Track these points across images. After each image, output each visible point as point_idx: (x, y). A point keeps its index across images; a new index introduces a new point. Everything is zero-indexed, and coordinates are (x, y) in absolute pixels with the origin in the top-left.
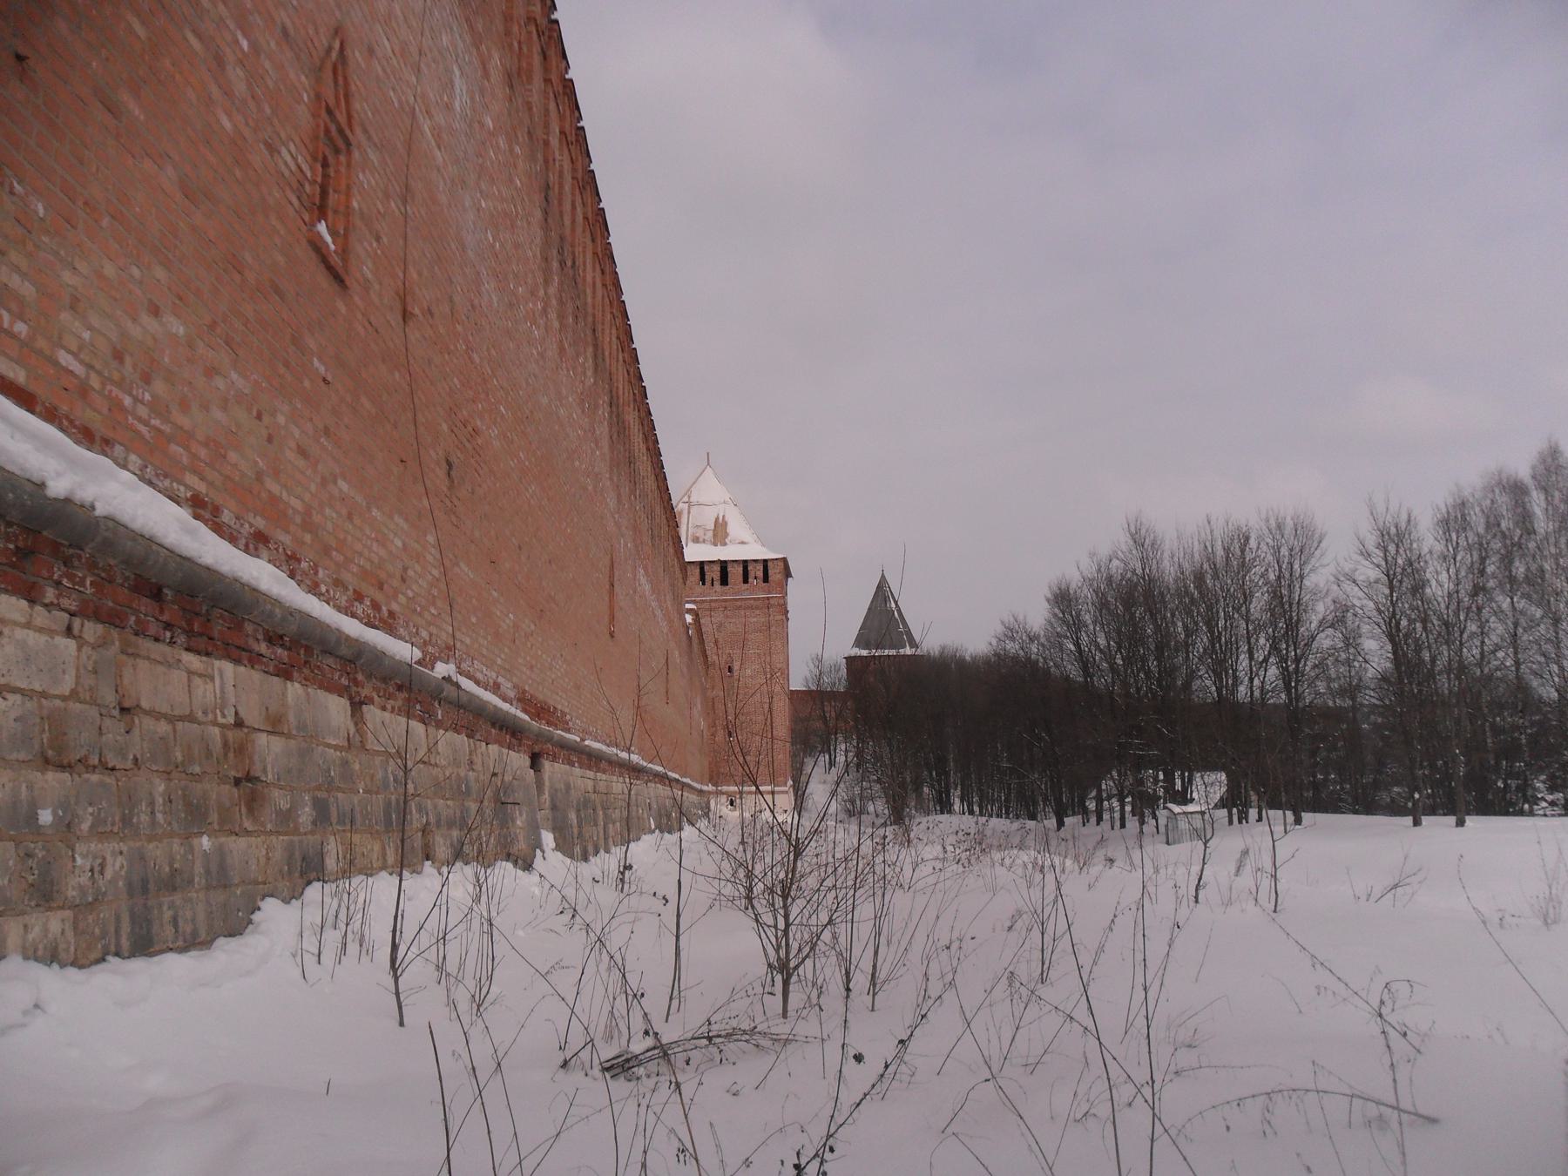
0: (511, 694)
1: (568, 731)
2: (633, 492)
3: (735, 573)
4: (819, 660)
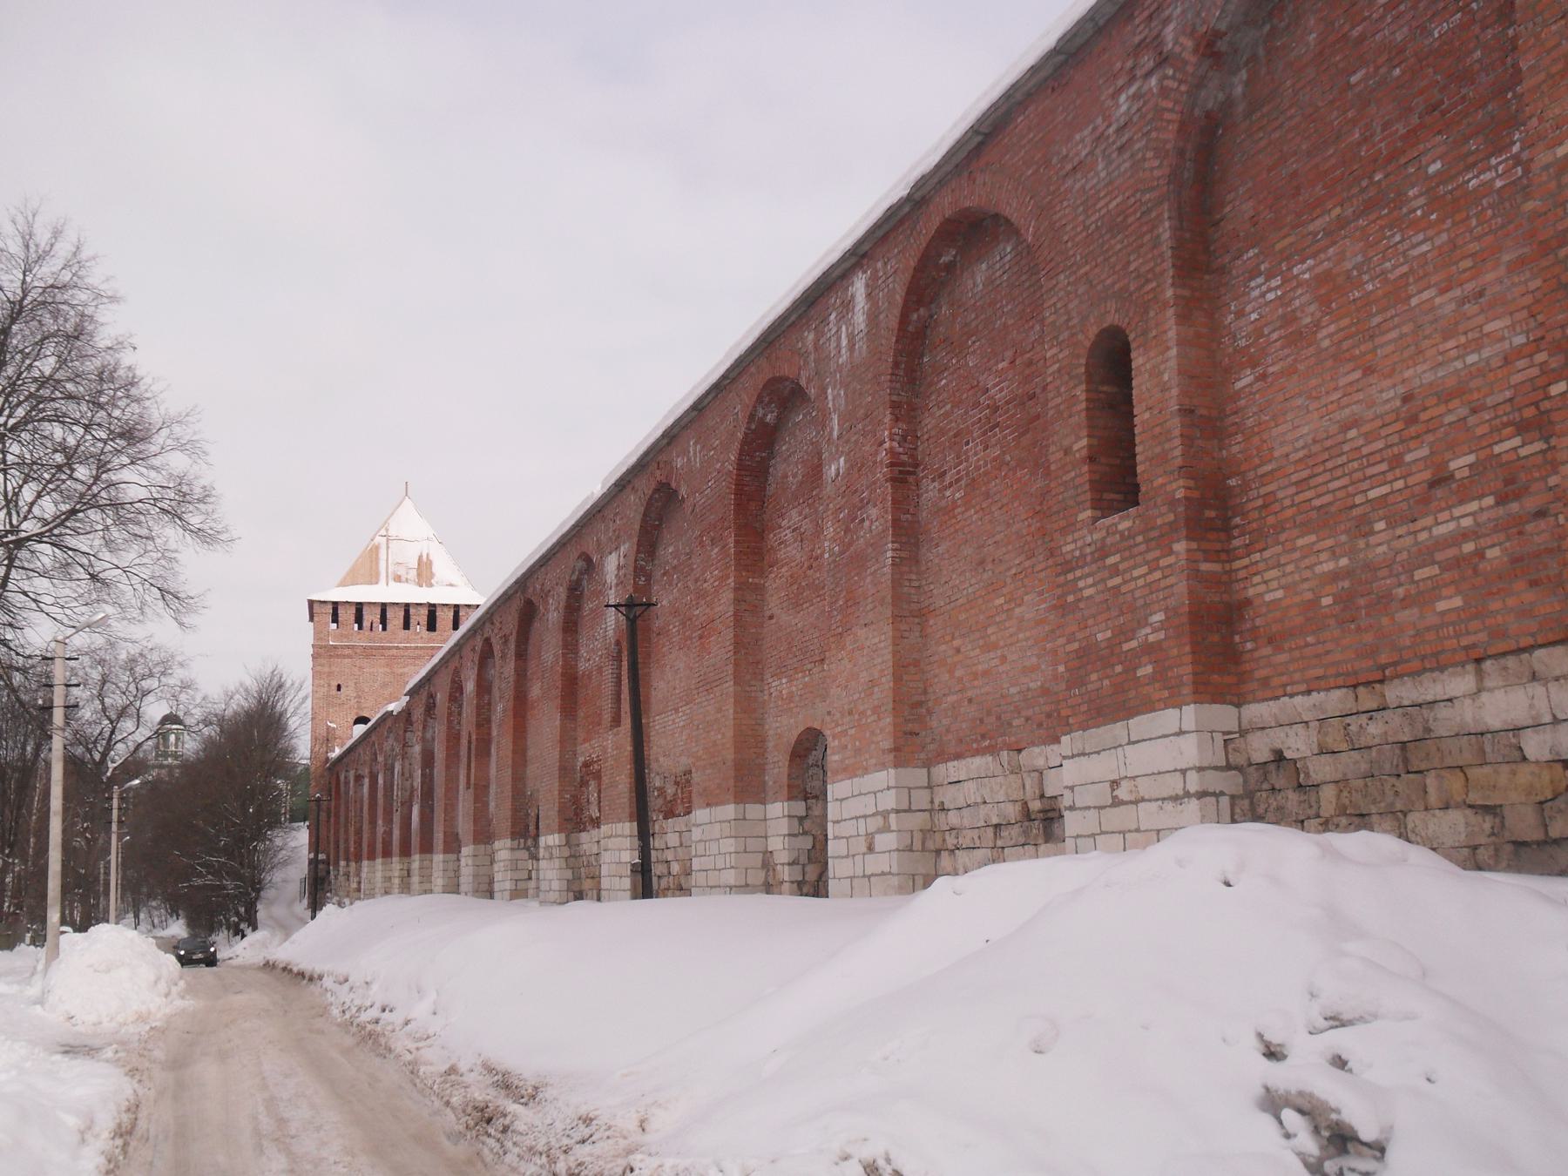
3: (371, 616)
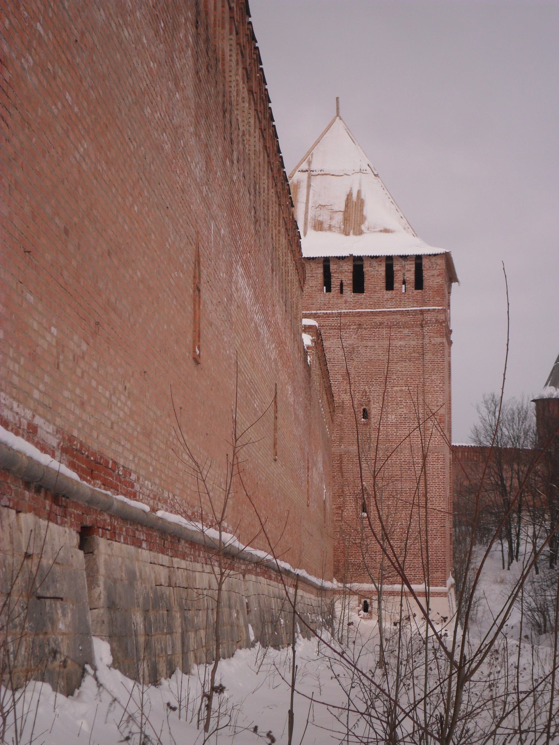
0: (53, 442)
1: (133, 496)
2: (228, 155)
3: (375, 275)
4: (496, 404)
